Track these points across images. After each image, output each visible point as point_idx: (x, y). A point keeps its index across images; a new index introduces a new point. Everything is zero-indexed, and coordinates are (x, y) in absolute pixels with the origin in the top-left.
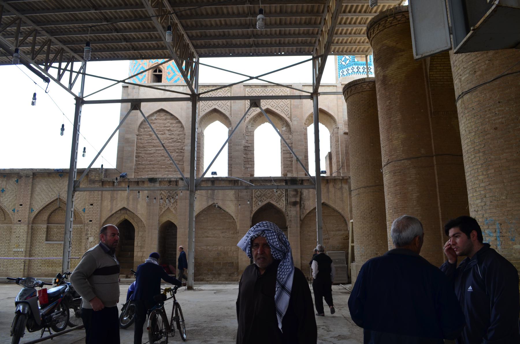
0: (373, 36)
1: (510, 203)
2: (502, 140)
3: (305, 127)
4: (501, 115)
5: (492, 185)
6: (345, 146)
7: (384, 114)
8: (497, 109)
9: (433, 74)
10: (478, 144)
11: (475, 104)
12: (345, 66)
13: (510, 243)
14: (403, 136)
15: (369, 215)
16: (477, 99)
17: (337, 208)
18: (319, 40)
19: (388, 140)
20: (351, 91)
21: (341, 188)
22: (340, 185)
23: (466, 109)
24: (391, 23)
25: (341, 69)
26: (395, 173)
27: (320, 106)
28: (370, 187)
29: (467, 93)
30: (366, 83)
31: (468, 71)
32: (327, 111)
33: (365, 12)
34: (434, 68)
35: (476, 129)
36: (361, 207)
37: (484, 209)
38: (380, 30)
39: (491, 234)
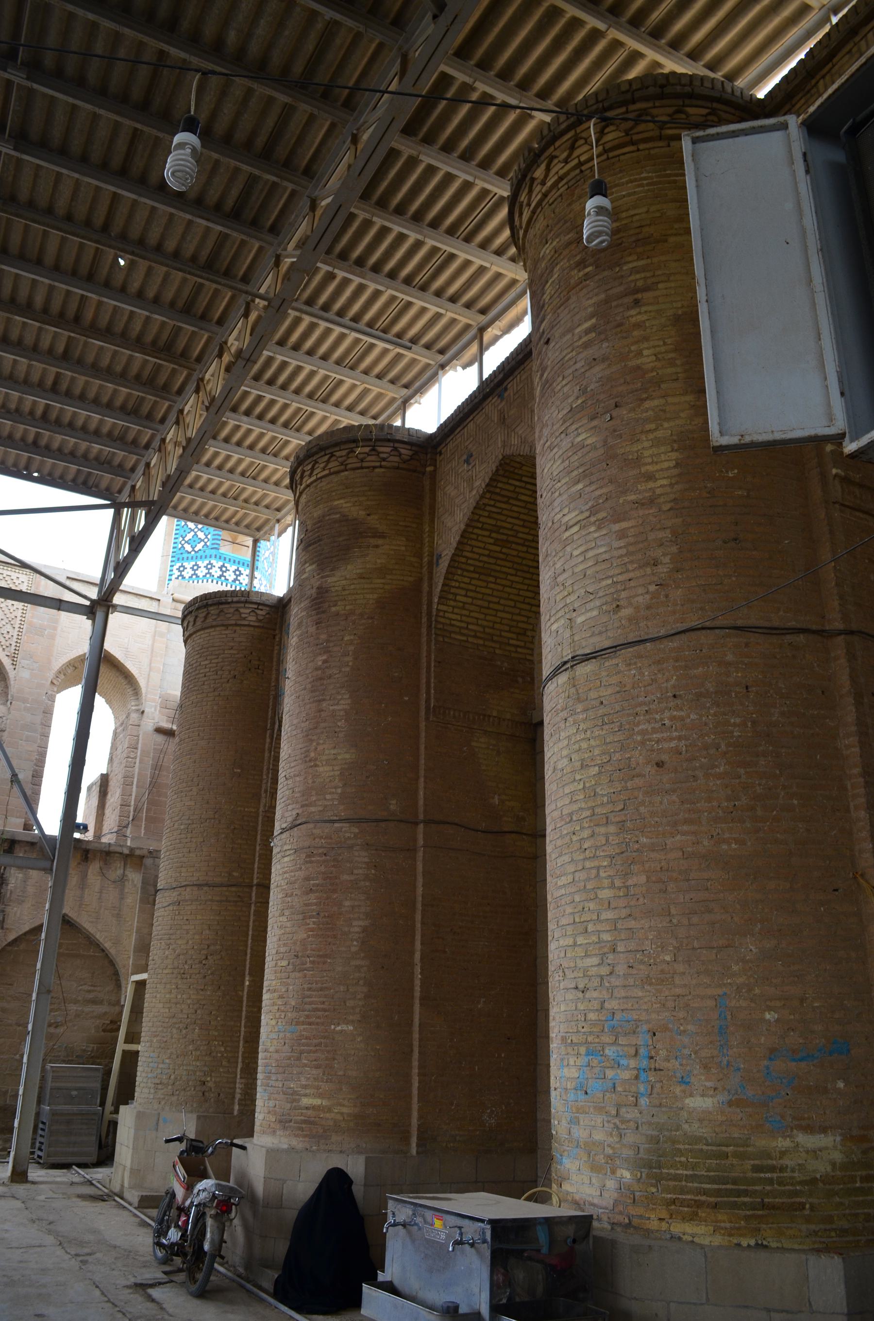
0: (307, 481)
1: (684, 973)
2: (674, 798)
3: (50, 692)
4: (676, 730)
5: (635, 919)
6: (152, 765)
7: (305, 689)
8: (667, 714)
9: (445, 612)
10: (605, 799)
11: (610, 691)
12: (190, 556)
13: (678, 1090)
14: (347, 756)
15: (197, 966)
16: (614, 680)
17: (99, 937)
18: (148, 465)
19: (306, 762)
20: (206, 618)
21: (123, 879)
22: (120, 872)
23: (579, 700)
24: (362, 461)
25: (178, 559)
26: (312, 855)
27: (107, 646)
28: (214, 886)
29: (588, 660)
30: (251, 606)
31: (598, 603)
32: (122, 661)
33: (286, 425)
34: (451, 596)
35: (605, 758)
36: (179, 942)
37: (607, 984)
38: (332, 470)
39: (624, 1062)
